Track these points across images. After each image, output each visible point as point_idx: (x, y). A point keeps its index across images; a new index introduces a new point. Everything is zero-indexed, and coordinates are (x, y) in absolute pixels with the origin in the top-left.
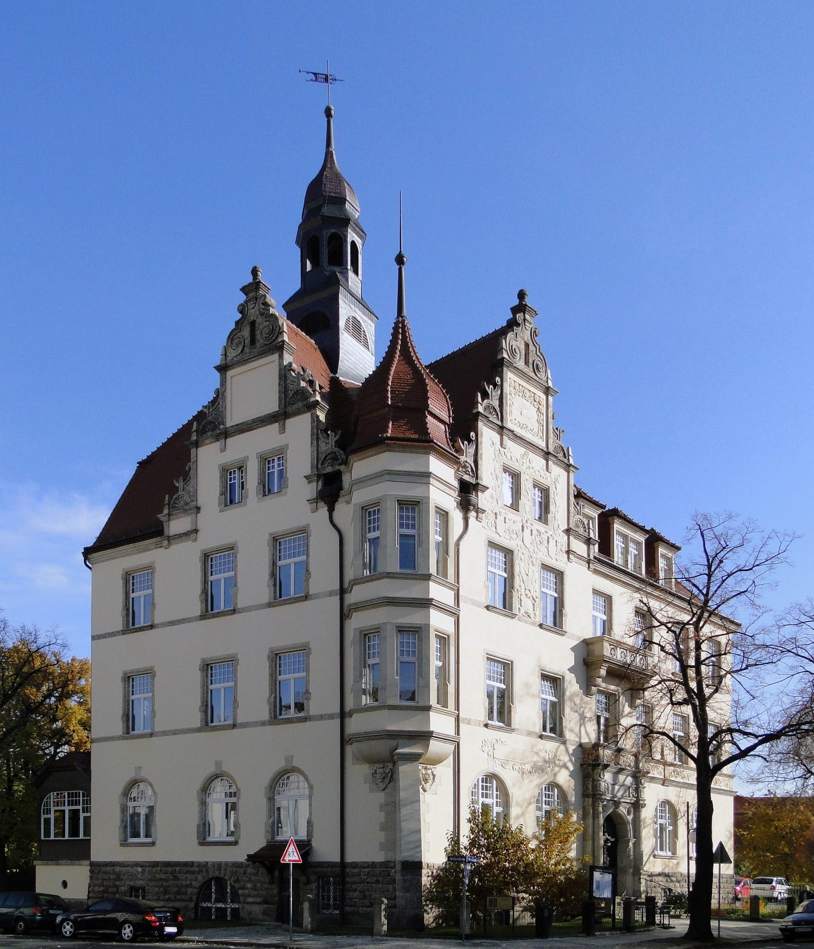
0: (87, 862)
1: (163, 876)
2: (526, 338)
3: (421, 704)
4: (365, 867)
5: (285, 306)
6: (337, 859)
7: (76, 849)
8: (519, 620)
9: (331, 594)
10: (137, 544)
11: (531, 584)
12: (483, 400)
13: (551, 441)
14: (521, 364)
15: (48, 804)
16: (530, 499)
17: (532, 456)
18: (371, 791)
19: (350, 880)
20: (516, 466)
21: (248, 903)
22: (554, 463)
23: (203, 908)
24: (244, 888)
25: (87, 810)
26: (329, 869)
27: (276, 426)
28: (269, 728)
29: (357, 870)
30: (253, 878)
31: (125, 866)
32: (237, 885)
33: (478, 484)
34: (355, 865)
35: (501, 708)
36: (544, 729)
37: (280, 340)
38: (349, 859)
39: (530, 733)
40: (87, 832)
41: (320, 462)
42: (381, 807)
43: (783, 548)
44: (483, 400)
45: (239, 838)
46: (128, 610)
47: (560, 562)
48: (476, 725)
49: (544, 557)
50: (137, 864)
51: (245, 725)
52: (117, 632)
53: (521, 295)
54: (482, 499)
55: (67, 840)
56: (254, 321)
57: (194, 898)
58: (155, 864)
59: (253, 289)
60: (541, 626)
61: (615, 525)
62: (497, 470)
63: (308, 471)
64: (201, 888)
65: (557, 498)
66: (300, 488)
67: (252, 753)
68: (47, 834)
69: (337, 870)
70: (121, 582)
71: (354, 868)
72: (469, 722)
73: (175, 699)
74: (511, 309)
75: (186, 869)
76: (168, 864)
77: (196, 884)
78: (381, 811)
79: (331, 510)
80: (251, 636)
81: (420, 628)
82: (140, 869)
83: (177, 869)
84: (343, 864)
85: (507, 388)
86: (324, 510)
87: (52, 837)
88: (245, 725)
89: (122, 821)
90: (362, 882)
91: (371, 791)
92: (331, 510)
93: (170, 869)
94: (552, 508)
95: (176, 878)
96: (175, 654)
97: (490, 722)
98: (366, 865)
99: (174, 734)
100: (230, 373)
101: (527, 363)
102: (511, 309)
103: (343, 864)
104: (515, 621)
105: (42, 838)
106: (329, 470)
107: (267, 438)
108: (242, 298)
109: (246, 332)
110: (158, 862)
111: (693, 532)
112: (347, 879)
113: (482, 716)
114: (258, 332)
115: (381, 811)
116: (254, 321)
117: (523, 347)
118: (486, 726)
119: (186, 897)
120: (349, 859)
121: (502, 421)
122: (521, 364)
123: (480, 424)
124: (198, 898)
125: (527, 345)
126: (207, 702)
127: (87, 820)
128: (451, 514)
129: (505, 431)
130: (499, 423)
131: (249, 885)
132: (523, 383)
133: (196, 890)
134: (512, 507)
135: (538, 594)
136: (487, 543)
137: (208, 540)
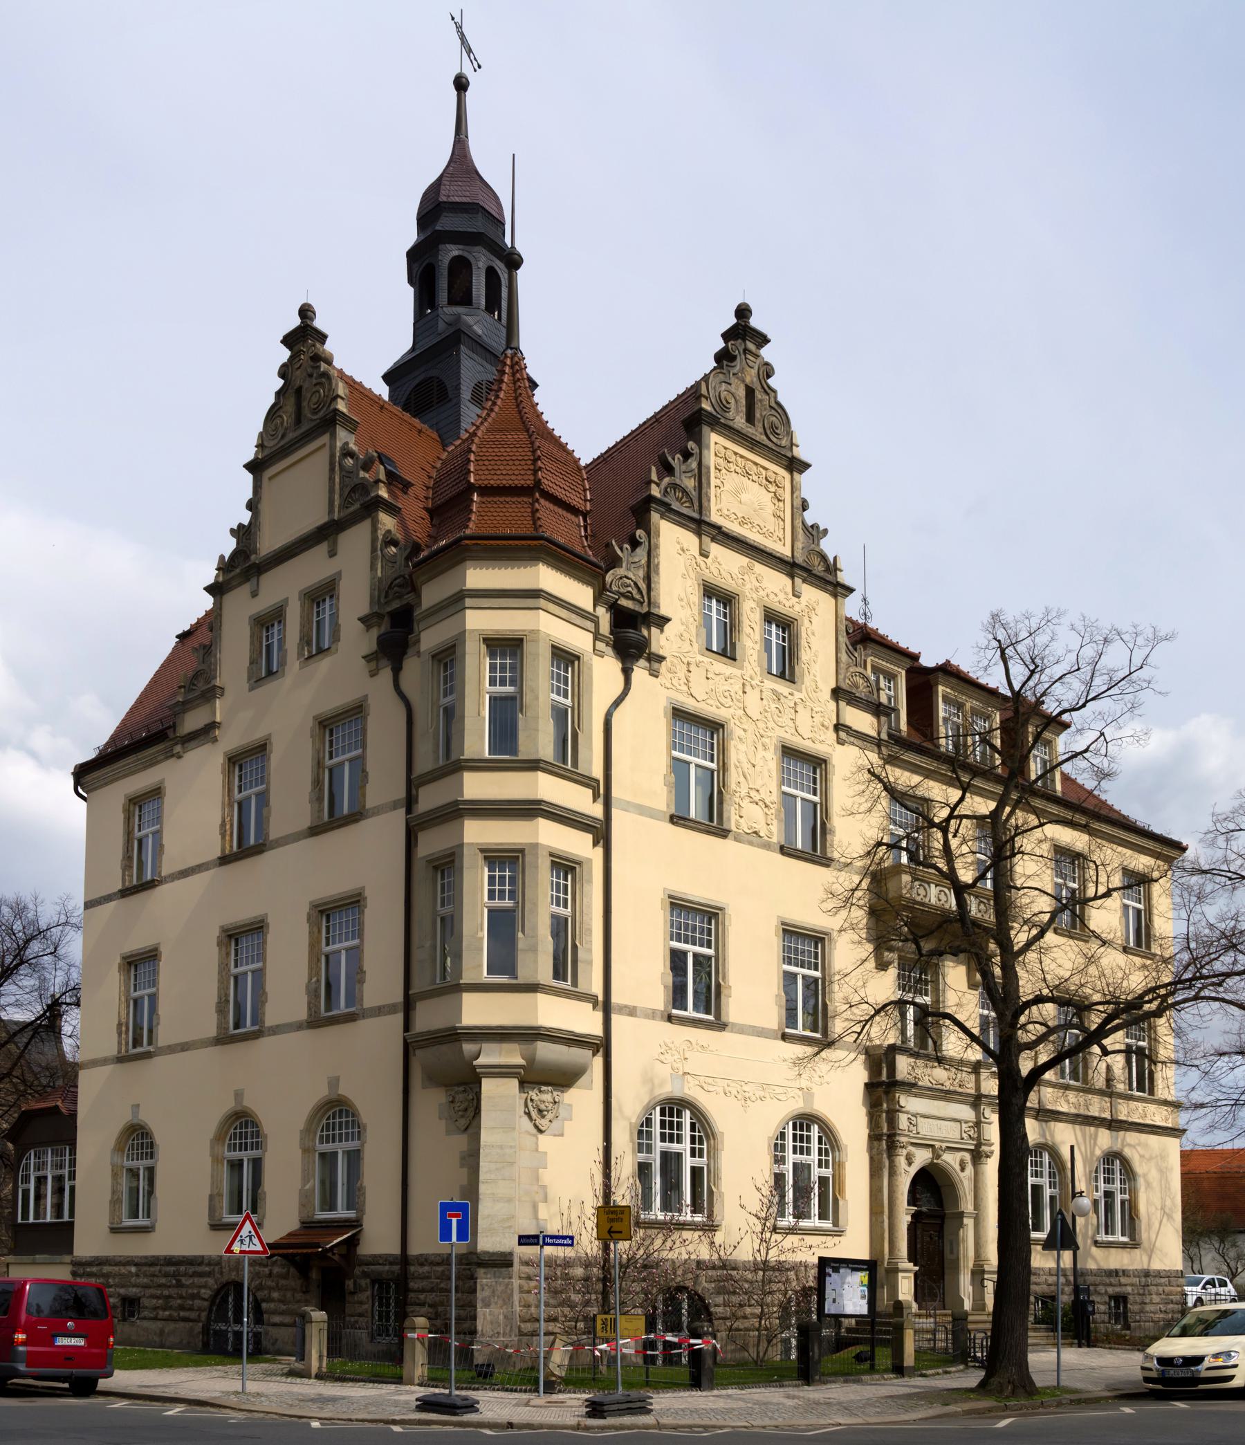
0: (67, 1259)
1: (163, 1281)
2: (748, 380)
3: (521, 980)
4: (438, 1264)
5: (388, 378)
6: (395, 1250)
7: (59, 1237)
8: (736, 839)
9: (394, 806)
10: (140, 755)
11: (755, 777)
12: (661, 478)
13: (799, 545)
14: (739, 422)
15: (27, 1167)
16: (753, 635)
17: (759, 568)
18: (448, 1132)
19: (416, 1286)
21: (275, 1325)
22: (804, 581)
24: (269, 1300)
25: (72, 1176)
26: (387, 1268)
27: (323, 548)
28: (306, 1034)
29: (426, 1268)
30: (283, 1282)
31: (116, 1265)
32: (260, 1295)
33: (649, 614)
34: (423, 1260)
38: (415, 1250)
39: (652, 1015)
40: (72, 1214)
41: (383, 595)
42: (463, 1158)
43: (1137, 662)
44: (661, 478)
45: (264, 1217)
46: (130, 858)
47: (823, 743)
48: (647, 1016)
49: (788, 736)
51: (275, 1030)
52: (114, 894)
53: (743, 312)
55: (33, 1224)
57: (204, 1315)
58: (153, 1261)
59: (305, 338)
60: (783, 850)
61: (941, 688)
63: (364, 609)
64: (212, 1300)
65: (812, 639)
66: (355, 640)
67: (285, 1080)
69: (396, 1268)
70: (122, 816)
71: (422, 1265)
72: (632, 1012)
73: (188, 996)
75: (191, 1270)
76: (170, 1261)
77: (206, 1293)
78: (462, 1166)
79: (397, 671)
80: (284, 888)
82: (133, 1269)
83: (182, 1268)
84: (404, 1259)
85: (711, 460)
86: (386, 674)
87: (31, 1220)
88: (275, 1030)
89: (114, 1192)
90: (432, 1290)
91: (448, 1132)
92: (397, 671)
93: (172, 1269)
95: (179, 1285)
96: (183, 919)
98: (438, 1259)
99: (183, 1050)
100: (268, 473)
101: (750, 418)
103: (404, 1259)
105: (19, 1221)
106: (396, 605)
107: (312, 568)
108: (285, 354)
109: (290, 407)
111: (1019, 672)
113: (658, 998)
115: (462, 1166)
117: (741, 393)
118: (670, 1018)
120: (415, 1250)
121: (701, 513)
122: (739, 422)
123: (655, 516)
124: (208, 1318)
125: (750, 392)
126: (227, 995)
127: (73, 1189)
128: (585, 659)
129: (704, 527)
130: (696, 515)
131: (275, 1295)
133: (206, 1304)
134: (782, 675)
135: (775, 797)
136: (670, 712)
137: (231, 739)
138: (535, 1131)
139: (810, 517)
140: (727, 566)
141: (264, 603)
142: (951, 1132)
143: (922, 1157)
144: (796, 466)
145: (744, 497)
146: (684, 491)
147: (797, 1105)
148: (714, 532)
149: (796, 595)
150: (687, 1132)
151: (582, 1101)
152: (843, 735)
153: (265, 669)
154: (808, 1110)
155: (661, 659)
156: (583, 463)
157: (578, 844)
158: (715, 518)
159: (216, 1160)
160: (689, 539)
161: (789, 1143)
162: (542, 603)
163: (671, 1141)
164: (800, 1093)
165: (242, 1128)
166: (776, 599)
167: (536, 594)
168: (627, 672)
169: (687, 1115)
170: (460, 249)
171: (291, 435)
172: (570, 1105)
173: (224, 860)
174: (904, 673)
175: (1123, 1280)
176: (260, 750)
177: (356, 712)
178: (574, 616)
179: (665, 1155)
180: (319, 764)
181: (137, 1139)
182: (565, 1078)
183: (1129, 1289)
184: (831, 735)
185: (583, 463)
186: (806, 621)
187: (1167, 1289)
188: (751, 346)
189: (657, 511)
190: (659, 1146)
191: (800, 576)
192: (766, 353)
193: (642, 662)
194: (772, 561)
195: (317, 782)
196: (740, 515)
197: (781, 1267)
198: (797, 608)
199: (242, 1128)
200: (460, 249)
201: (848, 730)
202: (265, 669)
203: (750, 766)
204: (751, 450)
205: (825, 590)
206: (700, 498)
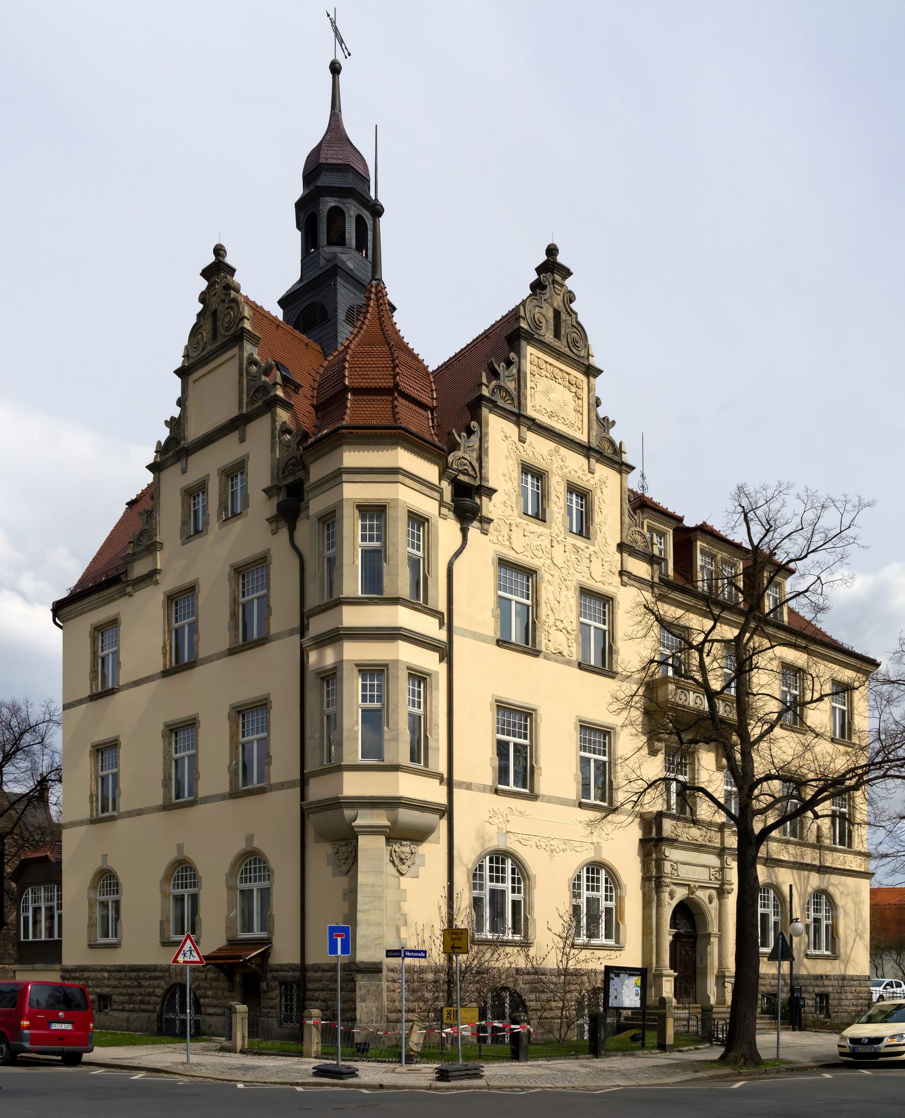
0: (58, 967)
1: (128, 983)
2: (555, 305)
4: (328, 971)
6: (297, 960)
8: (545, 658)
9: (291, 632)
11: (560, 610)
12: (489, 381)
13: (594, 433)
14: (549, 337)
15: (26, 900)
16: (558, 502)
17: (564, 451)
18: (334, 875)
20: (539, 463)
21: (210, 1014)
22: (597, 461)
23: (167, 1020)
24: (205, 996)
25: (60, 907)
27: (235, 435)
29: (319, 974)
30: (215, 984)
32: (198, 993)
33: (480, 486)
34: (317, 968)
35: (516, 769)
36: (586, 791)
37: (240, 326)
40: (60, 935)
41: (281, 472)
42: (345, 894)
44: (489, 381)
45: (200, 936)
47: (610, 585)
48: (479, 790)
50: (103, 969)
53: (552, 251)
54: (490, 507)
55: (32, 942)
56: (216, 311)
57: (158, 1007)
58: (120, 969)
59: (218, 271)
60: (581, 666)
62: (598, 491)
65: (603, 506)
66: (260, 507)
68: (26, 935)
69: (297, 974)
71: (316, 971)
72: (468, 786)
73: (141, 774)
74: (536, 269)
75: (148, 975)
76: (133, 968)
77: (159, 992)
78: (344, 900)
79: (292, 530)
80: (211, 692)
81: (386, 665)
82: (106, 975)
83: (141, 974)
84: (303, 967)
85: (528, 367)
86: (284, 533)
87: (31, 939)
89: (90, 918)
90: (323, 990)
91: (334, 875)
92: (292, 530)
93: (134, 974)
94: (597, 518)
97: (500, 786)
98: (328, 968)
99: (138, 815)
101: (557, 335)
102: (536, 269)
103: (303, 967)
104: (540, 660)
105: (22, 939)
106: (290, 479)
107: (226, 452)
108: (203, 284)
110: (123, 966)
111: (757, 531)
112: (309, 986)
114: (219, 323)
115: (344, 900)
116: (216, 311)
117: (550, 314)
119: (150, 1007)
121: (519, 408)
122: (549, 337)
124: (161, 1010)
125: (557, 314)
126: (170, 774)
127: (60, 916)
128: (432, 521)
130: (516, 410)
131: (210, 993)
132: (541, 355)
136: (496, 561)
137: (169, 582)
138: (397, 874)
139: (602, 412)
140: (540, 449)
141: (192, 477)
142: (702, 875)
143: (681, 893)
144: (591, 372)
145: (552, 396)
146: (507, 391)
147: (589, 855)
148: (530, 423)
149: (591, 472)
150: (509, 875)
151: (433, 852)
152: (625, 579)
153: (193, 530)
154: (598, 859)
155: (489, 521)
156: (430, 370)
157: (428, 660)
158: (530, 412)
159: (165, 895)
160: (511, 429)
161: (584, 883)
162: (400, 478)
163: (497, 881)
164: (592, 846)
165: (183, 872)
166: (576, 475)
167: (396, 471)
168: (464, 531)
169: (509, 862)
170: (336, 200)
171: (209, 348)
172: (423, 855)
173: (166, 673)
174: (671, 531)
175: (826, 983)
176: (191, 590)
177: (262, 561)
178: (424, 488)
179: (493, 892)
180: (235, 601)
181: (107, 880)
182: (419, 835)
183: (830, 989)
184: (617, 579)
185: (430, 370)
186: (598, 491)
187: (858, 989)
188: (558, 278)
189: (487, 407)
190: (585, 894)
191: (594, 457)
192: (570, 283)
193: (476, 524)
194: (574, 446)
195: (234, 615)
196: (549, 410)
197: (577, 973)
198: (592, 482)
199: (183, 872)
200: (336, 200)
201: (630, 575)
202: (193, 530)
203: (556, 603)
204: (558, 359)
205: (613, 468)
206: (519, 397)
